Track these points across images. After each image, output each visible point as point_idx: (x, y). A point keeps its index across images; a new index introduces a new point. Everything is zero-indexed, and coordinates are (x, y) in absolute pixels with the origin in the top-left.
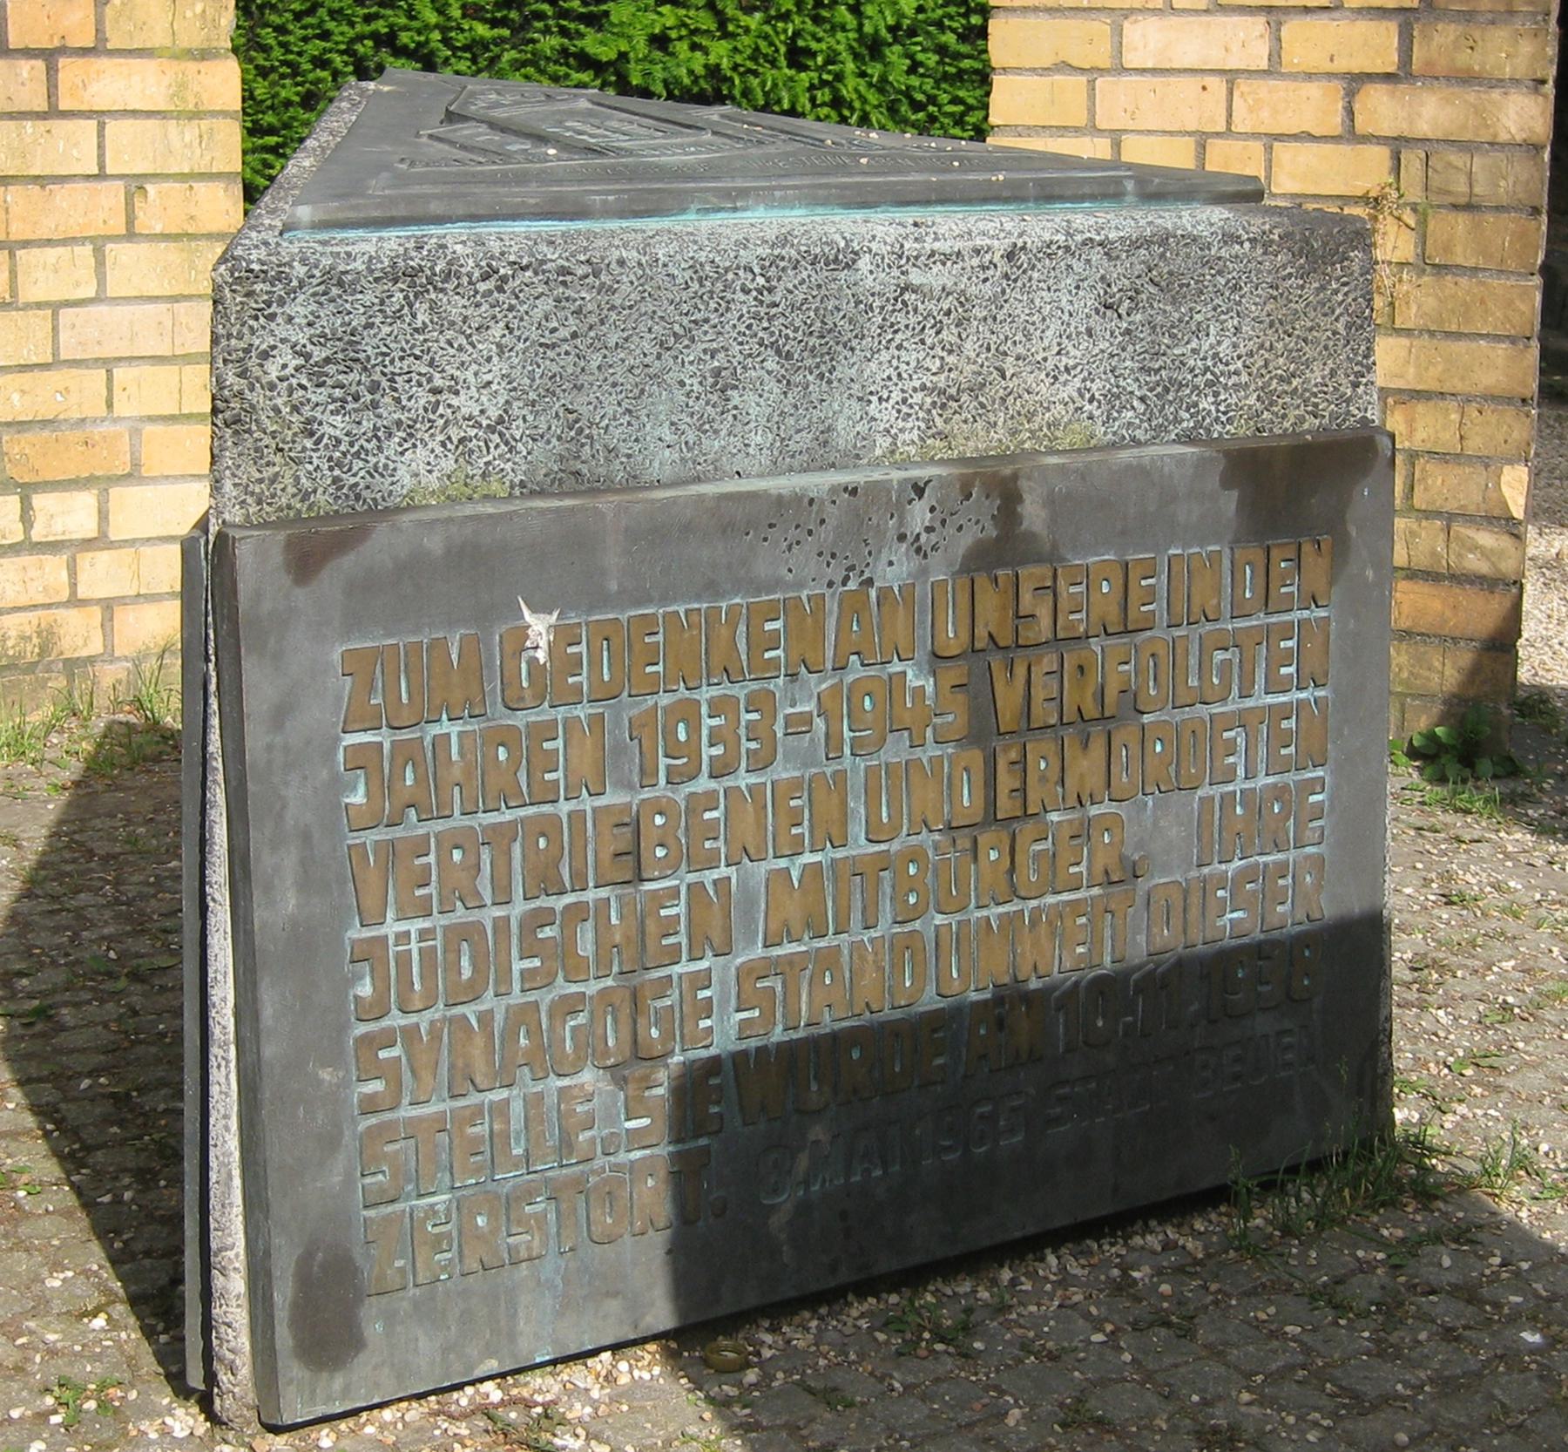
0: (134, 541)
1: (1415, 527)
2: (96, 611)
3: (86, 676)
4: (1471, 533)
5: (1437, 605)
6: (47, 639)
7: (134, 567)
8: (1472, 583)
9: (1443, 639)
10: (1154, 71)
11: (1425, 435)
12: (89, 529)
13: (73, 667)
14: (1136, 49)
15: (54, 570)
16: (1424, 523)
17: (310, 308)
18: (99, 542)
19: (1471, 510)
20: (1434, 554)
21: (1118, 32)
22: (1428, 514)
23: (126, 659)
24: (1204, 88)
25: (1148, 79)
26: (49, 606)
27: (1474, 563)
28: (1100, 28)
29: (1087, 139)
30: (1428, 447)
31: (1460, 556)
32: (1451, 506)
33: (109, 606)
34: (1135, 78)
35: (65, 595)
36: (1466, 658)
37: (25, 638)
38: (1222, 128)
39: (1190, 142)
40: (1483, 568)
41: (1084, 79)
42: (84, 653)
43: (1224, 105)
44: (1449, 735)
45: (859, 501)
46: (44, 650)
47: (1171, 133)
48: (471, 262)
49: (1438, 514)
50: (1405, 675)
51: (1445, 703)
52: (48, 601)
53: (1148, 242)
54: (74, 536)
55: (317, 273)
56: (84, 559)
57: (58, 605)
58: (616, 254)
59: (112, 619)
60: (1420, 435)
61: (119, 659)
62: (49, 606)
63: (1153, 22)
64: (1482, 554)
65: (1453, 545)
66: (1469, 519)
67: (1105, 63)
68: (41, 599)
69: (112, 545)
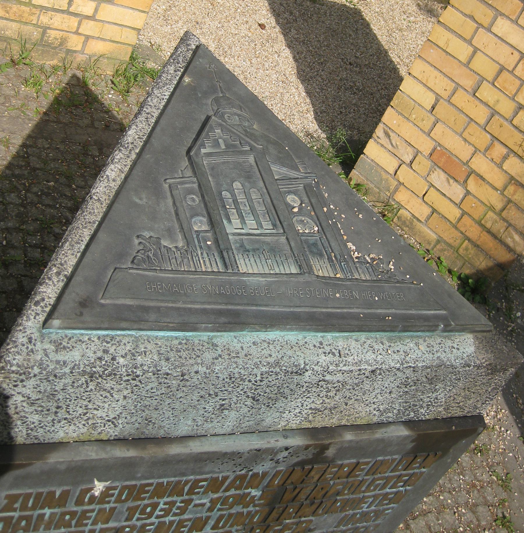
0: (104, 21)
1: (498, 220)
2: (83, 38)
3: (72, 56)
4: (514, 233)
5: (491, 245)
6: (63, 41)
7: (101, 29)
8: (505, 246)
9: (487, 254)
10: (499, 38)
11: (517, 198)
12: (90, 13)
13: (69, 52)
14: (498, 27)
15: (74, 22)
16: (501, 221)
17: (36, 383)
18: (92, 18)
19: (518, 227)
20: (499, 231)
21: (495, 19)
22: (504, 220)
23: (87, 54)
24: (512, 54)
25: (496, 39)
26: (68, 32)
27: (509, 241)
28: (491, 13)
29: (466, 45)
30: (516, 202)
31: (506, 236)
32: (512, 222)
33: (88, 38)
34: (492, 36)
35: (74, 30)
36: (490, 264)
37: (56, 38)
38: (510, 69)
39: (498, 67)
40: (511, 245)
41: (476, 25)
42: (74, 49)
43: (515, 63)
44: (472, 283)
45: (259, 453)
46: (61, 44)
47: (494, 60)
48: (124, 370)
49: (507, 221)
50: (470, 256)
51: (477, 271)
52: (68, 30)
53: (429, 367)
54: (84, 14)
55: (44, 372)
56: (85, 22)
57: (71, 32)
58: (196, 368)
59: (87, 42)
60: (516, 197)
61: (85, 54)
62: (68, 32)
63: (508, 22)
64: (513, 241)
65: (506, 233)
66: (516, 230)
67: (486, 25)
68: (66, 29)
69: (96, 20)
